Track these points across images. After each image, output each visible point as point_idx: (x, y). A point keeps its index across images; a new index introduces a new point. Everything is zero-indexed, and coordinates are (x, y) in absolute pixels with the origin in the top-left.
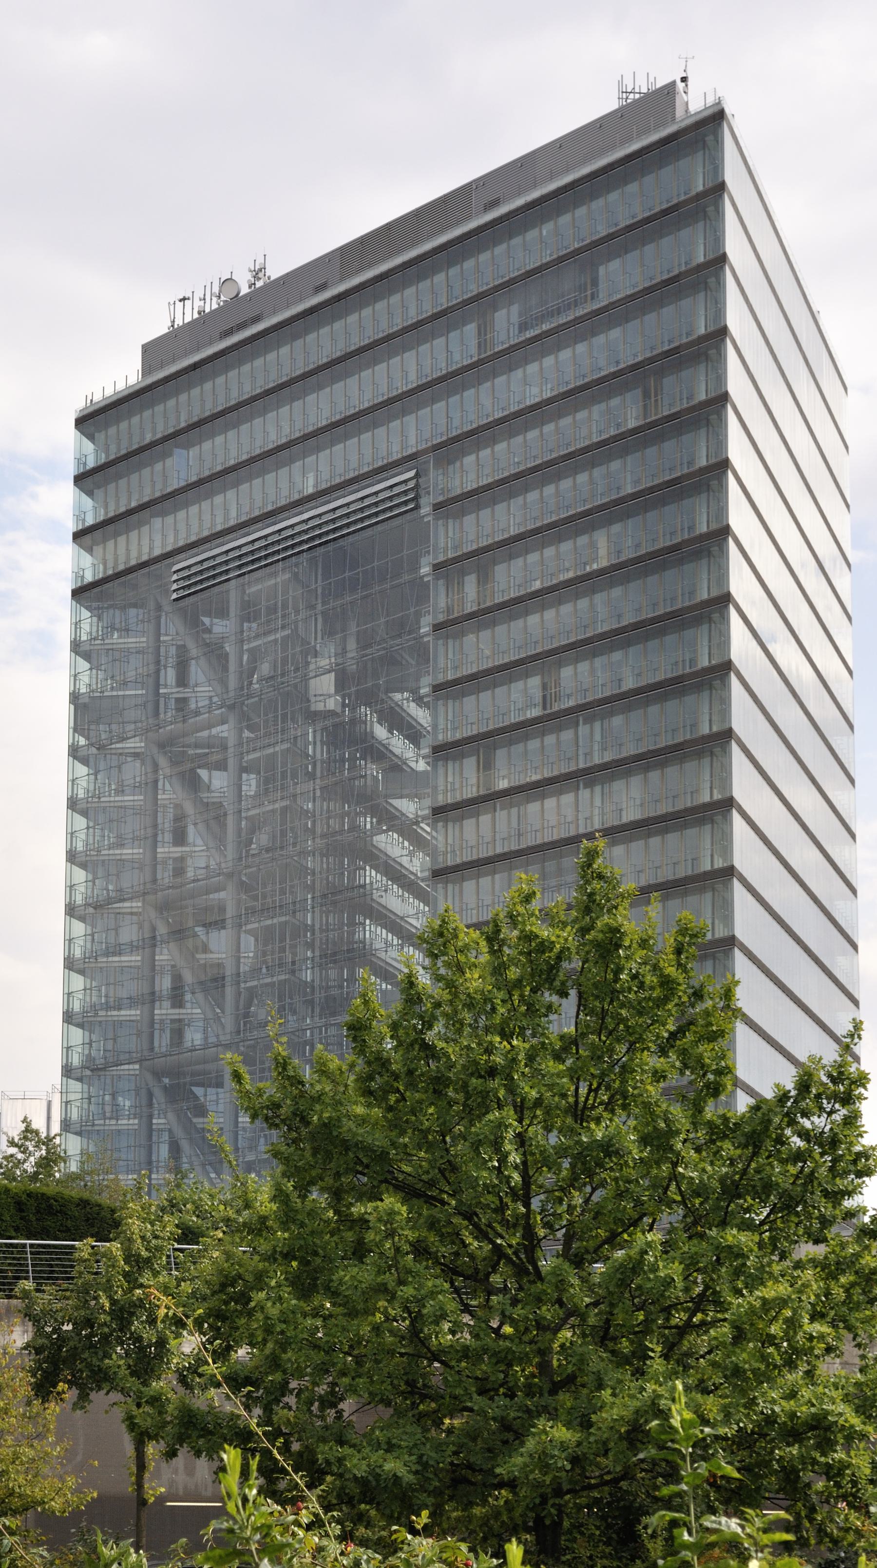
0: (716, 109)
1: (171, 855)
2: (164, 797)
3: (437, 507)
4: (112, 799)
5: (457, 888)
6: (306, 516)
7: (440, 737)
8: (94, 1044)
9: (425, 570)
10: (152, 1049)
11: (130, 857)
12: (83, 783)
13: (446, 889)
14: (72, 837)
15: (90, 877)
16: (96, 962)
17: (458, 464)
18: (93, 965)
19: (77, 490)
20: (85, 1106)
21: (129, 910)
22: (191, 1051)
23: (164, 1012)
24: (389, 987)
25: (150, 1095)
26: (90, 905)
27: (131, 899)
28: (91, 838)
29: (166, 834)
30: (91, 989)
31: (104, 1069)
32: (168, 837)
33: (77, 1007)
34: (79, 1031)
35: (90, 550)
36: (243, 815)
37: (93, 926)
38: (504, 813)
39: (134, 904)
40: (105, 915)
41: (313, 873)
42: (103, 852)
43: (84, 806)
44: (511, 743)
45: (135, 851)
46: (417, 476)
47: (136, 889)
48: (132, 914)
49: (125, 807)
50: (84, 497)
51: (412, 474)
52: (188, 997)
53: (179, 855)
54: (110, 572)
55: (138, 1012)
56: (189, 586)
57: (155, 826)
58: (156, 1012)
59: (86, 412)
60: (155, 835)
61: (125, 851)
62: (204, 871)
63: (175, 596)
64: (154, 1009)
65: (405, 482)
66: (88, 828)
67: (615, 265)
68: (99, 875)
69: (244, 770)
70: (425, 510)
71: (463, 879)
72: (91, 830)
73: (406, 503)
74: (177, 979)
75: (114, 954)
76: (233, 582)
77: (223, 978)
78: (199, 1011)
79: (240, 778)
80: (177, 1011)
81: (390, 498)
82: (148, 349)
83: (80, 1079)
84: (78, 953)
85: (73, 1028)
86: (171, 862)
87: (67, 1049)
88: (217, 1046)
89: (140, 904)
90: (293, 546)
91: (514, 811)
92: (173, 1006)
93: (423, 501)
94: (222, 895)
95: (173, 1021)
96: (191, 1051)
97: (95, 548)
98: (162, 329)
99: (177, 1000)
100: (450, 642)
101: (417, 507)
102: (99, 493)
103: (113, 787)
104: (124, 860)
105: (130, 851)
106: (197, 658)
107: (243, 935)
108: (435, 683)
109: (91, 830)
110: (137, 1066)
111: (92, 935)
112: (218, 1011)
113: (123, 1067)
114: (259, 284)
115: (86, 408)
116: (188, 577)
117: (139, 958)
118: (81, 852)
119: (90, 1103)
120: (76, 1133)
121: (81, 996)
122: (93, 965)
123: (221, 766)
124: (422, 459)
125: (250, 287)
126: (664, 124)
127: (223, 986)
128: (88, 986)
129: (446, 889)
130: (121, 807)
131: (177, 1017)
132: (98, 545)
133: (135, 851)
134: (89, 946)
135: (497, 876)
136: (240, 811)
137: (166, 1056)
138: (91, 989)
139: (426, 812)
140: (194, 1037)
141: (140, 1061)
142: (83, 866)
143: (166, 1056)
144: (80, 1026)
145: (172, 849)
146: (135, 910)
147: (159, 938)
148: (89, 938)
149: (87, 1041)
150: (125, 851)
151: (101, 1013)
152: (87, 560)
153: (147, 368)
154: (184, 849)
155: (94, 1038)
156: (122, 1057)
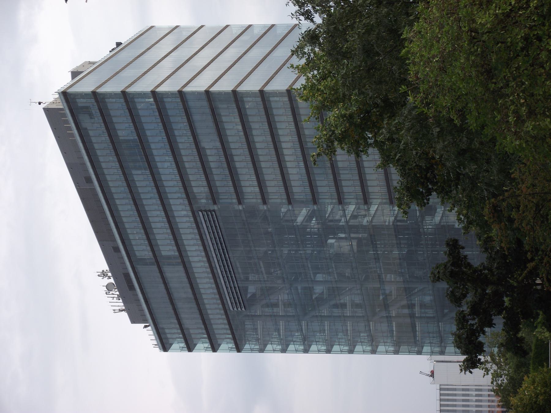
0: (61, 94)
1: (283, 309)
2: (258, 312)
3: (215, 203)
4: (327, 334)
5: (372, 194)
6: (214, 255)
7: (284, 201)
8: (362, 341)
9: (240, 207)
10: (363, 316)
11: (284, 326)
12: (253, 346)
13: (321, 199)
14: (253, 351)
15: (292, 343)
16: (328, 340)
17: (196, 194)
18: (329, 341)
19: (194, 351)
20: (434, 345)
21: (306, 326)
22: (364, 300)
23: (348, 312)
24: (314, 219)
25: (313, 316)
26: (304, 343)
27: (301, 326)
28: (276, 343)
29: (275, 311)
30: (339, 342)
31: (441, 337)
32: (275, 310)
33: (324, 348)
34: (379, 347)
35: (171, 345)
36: (266, 279)
37: (313, 341)
38: (342, 176)
39: (304, 324)
40: (308, 336)
41: (290, 251)
42: (282, 338)
43: (285, 346)
44: (237, 174)
45: (281, 324)
46: (201, 211)
47: (297, 323)
48: (307, 325)
49: (263, 328)
50: (197, 347)
51: (200, 213)
52: (342, 301)
53: (283, 306)
54: (181, 336)
55: (349, 322)
56: (240, 303)
57: (271, 316)
58: (348, 315)
59: (161, 347)
60: (274, 316)
61: (281, 329)
62: (289, 295)
63: (243, 309)
64: (347, 316)
65: (203, 215)
66: (272, 344)
67: (120, 133)
68: (291, 339)
69: (247, 279)
70: (216, 207)
71: (368, 192)
72: (273, 343)
73: (212, 215)
74: (403, 307)
75: (393, 333)
76: (239, 285)
77: (405, 288)
78: (416, 299)
79: (251, 281)
80: (348, 307)
81: (210, 221)
82: (134, 320)
83: (377, 347)
84: (324, 348)
85: (333, 350)
86: (286, 309)
87: (364, 352)
88: (361, 290)
89: (303, 322)
90: (226, 260)
91: (341, 172)
92: (278, 307)
93: (212, 209)
94: (299, 288)
95: (352, 308)
96: (364, 300)
97: (170, 343)
98: (125, 315)
99: (344, 306)
100: (245, 197)
101: (214, 211)
102: (171, 341)
103: (322, 334)
104: (285, 329)
105: (281, 326)
106: (270, 299)
107: (387, 280)
108: (262, 204)
109: (273, 343)
110: (371, 323)
111: (316, 342)
112: (348, 289)
113: (441, 329)
114: (110, 274)
115: (159, 347)
116: (236, 303)
117: (281, 322)
118: (282, 347)
119: (387, 342)
120: (423, 348)
121: (365, 347)
122: (329, 341)
123: (311, 289)
124: (195, 209)
125: (110, 278)
126: (64, 115)
127: (337, 287)
128: (338, 343)
129: (321, 199)
130: (263, 330)
131: (350, 306)
132: (217, 342)
133: (281, 324)
134: (321, 343)
135: (317, 179)
136: (265, 281)
137: (366, 311)
138: (339, 342)
139: (340, 207)
140: (358, 300)
141: (369, 321)
142: (287, 346)
143: (366, 311)
144: (354, 347)
145: (348, 310)
146: (306, 324)
147: (387, 315)
148: (317, 343)
149: (429, 345)
150: (281, 329)
151: (282, 338)
152: (175, 346)
153: (144, 321)
154: (280, 304)
155: (360, 341)
156: (367, 329)
